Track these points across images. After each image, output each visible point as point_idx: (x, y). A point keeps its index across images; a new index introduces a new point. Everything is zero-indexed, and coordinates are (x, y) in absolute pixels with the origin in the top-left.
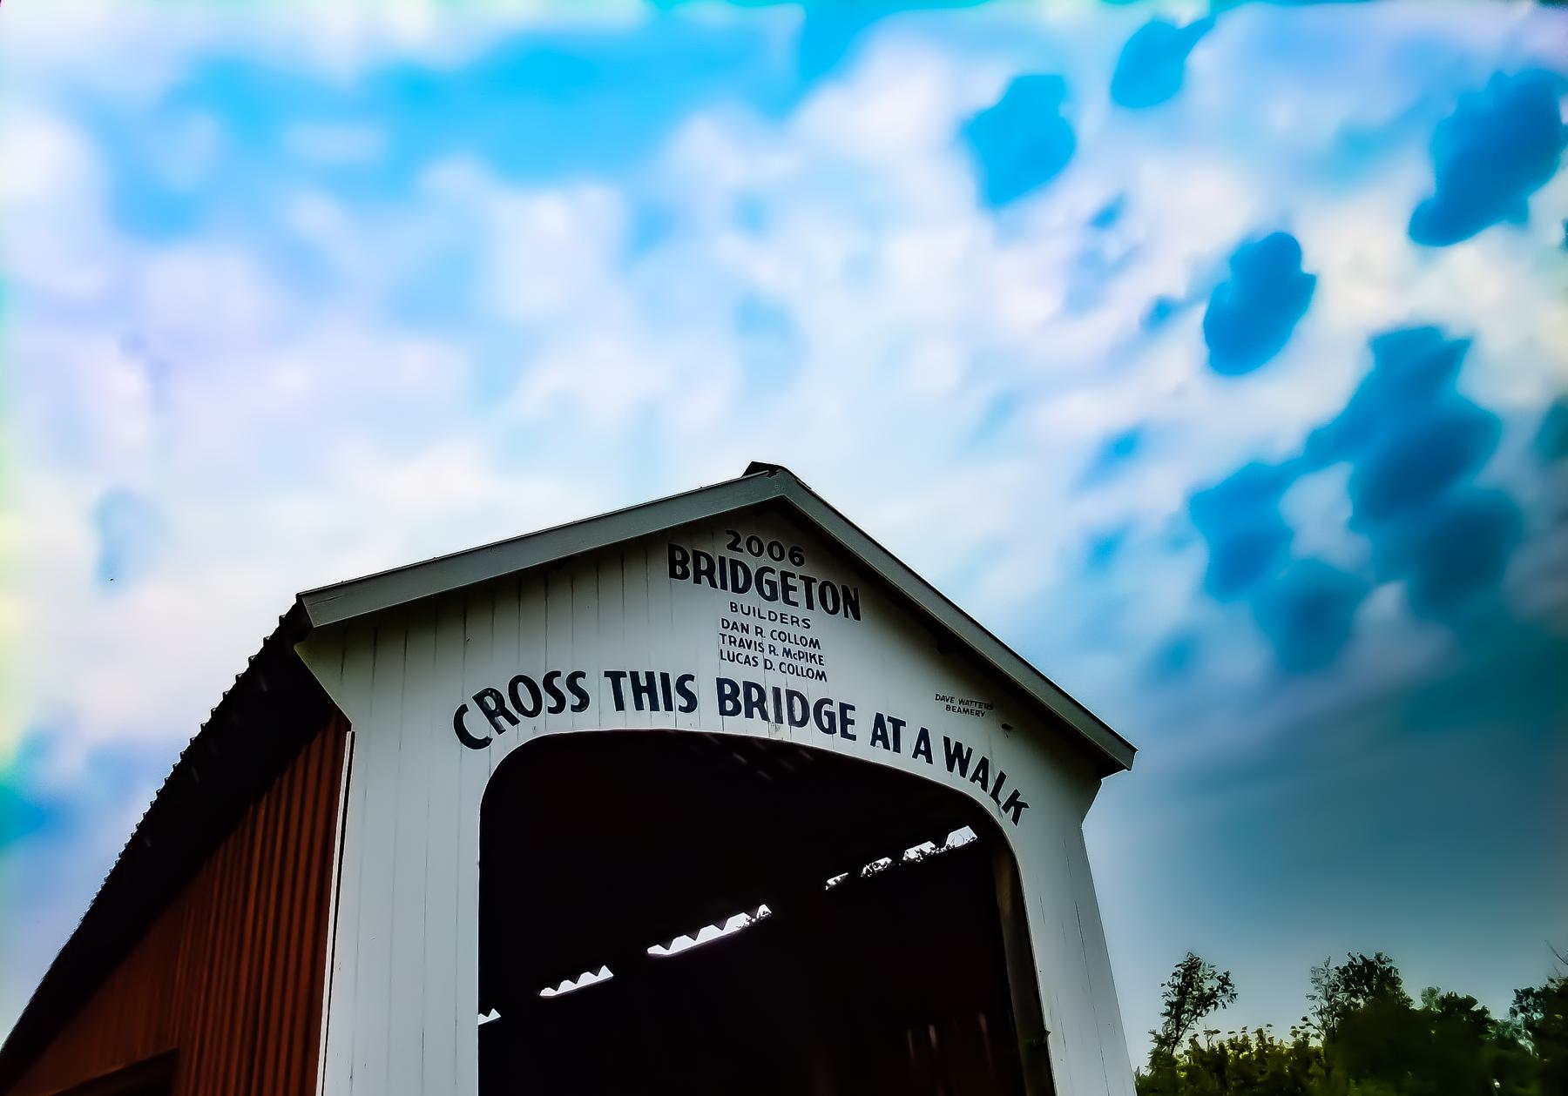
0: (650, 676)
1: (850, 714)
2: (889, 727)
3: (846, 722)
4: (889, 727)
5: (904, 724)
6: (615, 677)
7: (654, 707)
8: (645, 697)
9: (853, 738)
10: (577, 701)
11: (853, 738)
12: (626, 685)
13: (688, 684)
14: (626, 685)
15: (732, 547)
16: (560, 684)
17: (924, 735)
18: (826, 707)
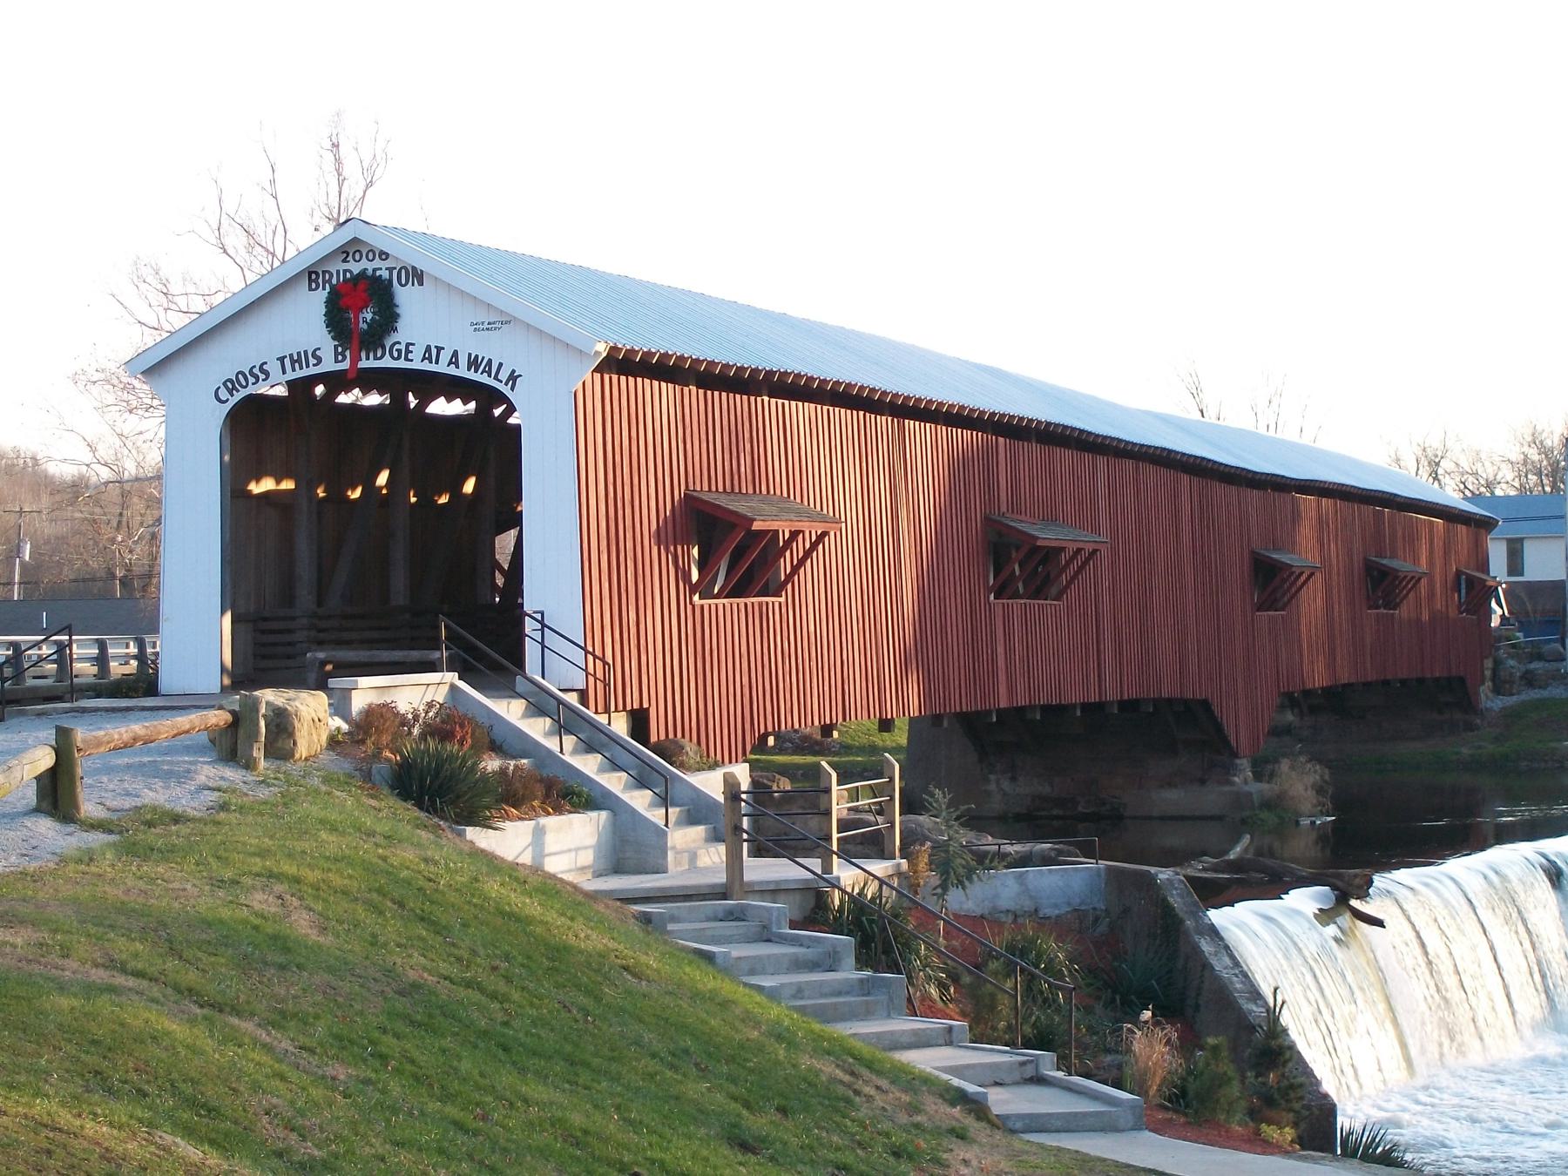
0: (299, 353)
1: (411, 348)
2: (434, 352)
3: (408, 351)
4: (434, 352)
5: (443, 349)
6: (282, 359)
7: (301, 368)
8: (297, 365)
9: (412, 360)
10: (264, 377)
11: (412, 360)
12: (287, 361)
13: (265, 367)
14: (287, 361)
15: (345, 261)
16: (256, 371)
17: (455, 354)
18: (397, 347)
